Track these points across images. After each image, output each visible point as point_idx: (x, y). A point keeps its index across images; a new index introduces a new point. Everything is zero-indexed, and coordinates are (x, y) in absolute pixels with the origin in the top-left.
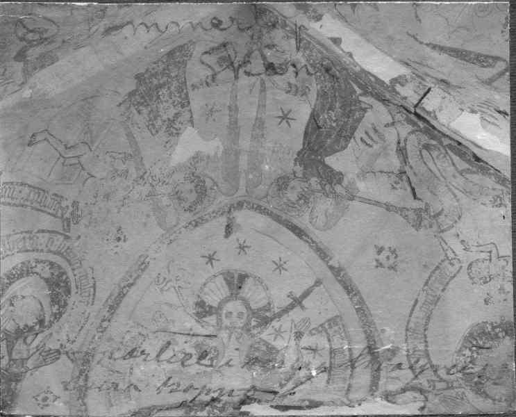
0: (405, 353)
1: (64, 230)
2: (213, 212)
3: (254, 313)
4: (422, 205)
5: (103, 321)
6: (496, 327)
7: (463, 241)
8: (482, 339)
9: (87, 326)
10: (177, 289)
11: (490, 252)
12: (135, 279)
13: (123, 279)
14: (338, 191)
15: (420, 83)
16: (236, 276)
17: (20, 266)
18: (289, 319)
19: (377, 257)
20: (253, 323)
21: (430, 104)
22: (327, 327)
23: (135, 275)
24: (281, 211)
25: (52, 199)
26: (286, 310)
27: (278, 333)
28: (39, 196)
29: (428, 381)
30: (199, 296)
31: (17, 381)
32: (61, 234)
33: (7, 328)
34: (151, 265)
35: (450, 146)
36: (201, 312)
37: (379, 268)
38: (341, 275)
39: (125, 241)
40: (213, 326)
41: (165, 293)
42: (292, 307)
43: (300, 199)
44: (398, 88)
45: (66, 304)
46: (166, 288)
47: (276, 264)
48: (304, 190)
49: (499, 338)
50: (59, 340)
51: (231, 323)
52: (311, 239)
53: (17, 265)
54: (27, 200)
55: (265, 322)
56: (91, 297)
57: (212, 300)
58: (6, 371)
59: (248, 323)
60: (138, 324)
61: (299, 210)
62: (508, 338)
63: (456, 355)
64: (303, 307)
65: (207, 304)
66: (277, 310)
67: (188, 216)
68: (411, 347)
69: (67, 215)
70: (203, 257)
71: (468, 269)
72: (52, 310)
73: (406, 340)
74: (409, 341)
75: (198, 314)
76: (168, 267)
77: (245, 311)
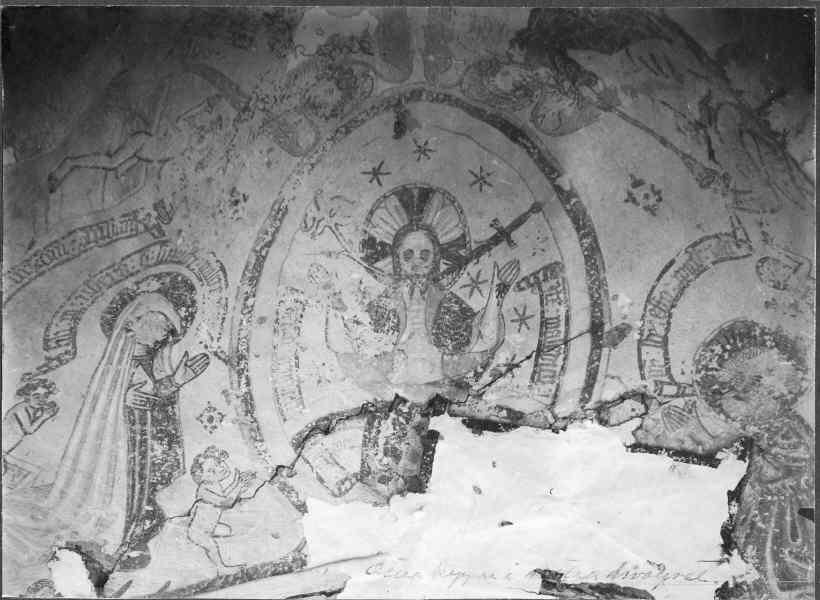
1: (155, 237)
2: (373, 108)
3: (444, 251)
5: (246, 299)
6: (767, 334)
7: (763, 233)
8: (741, 341)
9: (228, 317)
10: (334, 228)
11: (800, 264)
12: (273, 235)
13: (257, 242)
14: (585, 95)
16: (416, 192)
17: (118, 298)
18: (492, 260)
19: (630, 189)
20: (443, 268)
22: (541, 278)
23: (271, 230)
24: (484, 103)
25: (121, 223)
26: (485, 248)
27: (475, 284)
28: (102, 232)
29: (656, 382)
30: (366, 232)
31: (173, 404)
32: (155, 244)
33: (136, 354)
34: (292, 209)
36: (372, 254)
37: (630, 204)
38: (572, 203)
39: (245, 200)
40: (390, 274)
41: (317, 237)
42: (496, 240)
43: (517, 89)
45: (194, 302)
46: (319, 231)
47: (476, 176)
48: (525, 80)
49: (766, 346)
50: (201, 343)
51: (413, 269)
52: (532, 143)
53: (114, 298)
54: (89, 243)
55: (459, 264)
56: (223, 282)
57: (383, 233)
58: (156, 395)
59: (436, 267)
60: (292, 289)
61: (514, 102)
62: (776, 349)
64: (511, 243)
65: (378, 241)
66: (474, 246)
67: (334, 123)
68: (648, 326)
69: (153, 221)
70: (365, 173)
71: (760, 261)
72: (178, 314)
73: (643, 316)
74: (646, 319)
75: (366, 259)
76: (316, 202)
77: (430, 247)
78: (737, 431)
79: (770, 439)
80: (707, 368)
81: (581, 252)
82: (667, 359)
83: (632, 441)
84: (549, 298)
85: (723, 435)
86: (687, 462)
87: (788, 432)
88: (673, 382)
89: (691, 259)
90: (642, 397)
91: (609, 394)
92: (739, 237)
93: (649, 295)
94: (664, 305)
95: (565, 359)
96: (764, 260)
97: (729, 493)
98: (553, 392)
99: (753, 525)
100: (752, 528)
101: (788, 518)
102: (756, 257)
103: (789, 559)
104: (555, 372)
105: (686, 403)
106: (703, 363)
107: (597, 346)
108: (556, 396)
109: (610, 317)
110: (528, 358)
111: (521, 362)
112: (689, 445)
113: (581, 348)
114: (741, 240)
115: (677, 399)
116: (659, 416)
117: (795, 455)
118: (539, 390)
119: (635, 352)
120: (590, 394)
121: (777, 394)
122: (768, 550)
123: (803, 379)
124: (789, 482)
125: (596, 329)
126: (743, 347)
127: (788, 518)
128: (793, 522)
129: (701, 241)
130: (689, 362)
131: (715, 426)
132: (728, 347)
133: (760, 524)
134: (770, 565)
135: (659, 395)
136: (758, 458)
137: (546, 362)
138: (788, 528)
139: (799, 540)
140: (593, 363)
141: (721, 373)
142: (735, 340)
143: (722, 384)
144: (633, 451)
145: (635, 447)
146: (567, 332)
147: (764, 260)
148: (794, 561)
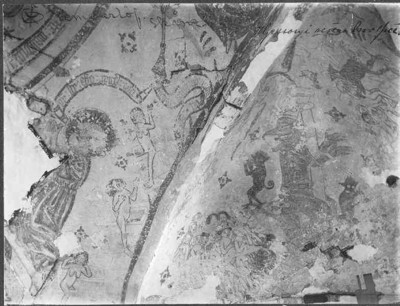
0: (68, 81)
4: (168, 78)
6: (109, 128)
8: (100, 121)
15: (242, 101)
21: (228, 111)
29: (58, 106)
35: (203, 114)
44: (237, 88)
63: (84, 109)
68: (75, 82)
71: (138, 108)
73: (78, 76)
78: (66, 149)
79: (74, 161)
80: (78, 119)
81: (82, 25)
82: (69, 101)
83: (31, 123)
84: (51, 25)
85: (61, 147)
86: (43, 148)
87: (81, 164)
88: (63, 112)
89: (114, 78)
90: (48, 106)
91: (39, 94)
92: (141, 95)
93: (87, 72)
94: (88, 81)
95: (34, 59)
96: (139, 109)
97: (46, 172)
98: (18, 68)
99: (42, 190)
100: (41, 191)
101: (56, 195)
102: (138, 106)
103: (45, 211)
104: (25, 59)
105: (60, 124)
106: (79, 115)
107: (51, 67)
108: (17, 71)
109: (66, 62)
110: (19, 39)
111: (14, 37)
112: (47, 142)
113: (43, 62)
114: (140, 97)
115: (59, 120)
116: (47, 120)
117: (76, 173)
118: (12, 60)
119: (62, 87)
120: (32, 86)
121: (91, 148)
122: (41, 203)
123: (104, 152)
124: (67, 182)
125: (57, 60)
126: (98, 124)
127: (56, 195)
128: (56, 197)
129: (126, 79)
130: (75, 110)
131: (60, 140)
132: (93, 119)
133: (45, 191)
134: (38, 210)
135: (54, 112)
136: (64, 165)
137: (25, 51)
138: (53, 199)
139: (54, 205)
140: (44, 73)
141: (81, 124)
142: (98, 118)
143: (77, 129)
144: (29, 128)
145: (31, 127)
146: (45, 48)
147: (139, 109)
148: (46, 213)
